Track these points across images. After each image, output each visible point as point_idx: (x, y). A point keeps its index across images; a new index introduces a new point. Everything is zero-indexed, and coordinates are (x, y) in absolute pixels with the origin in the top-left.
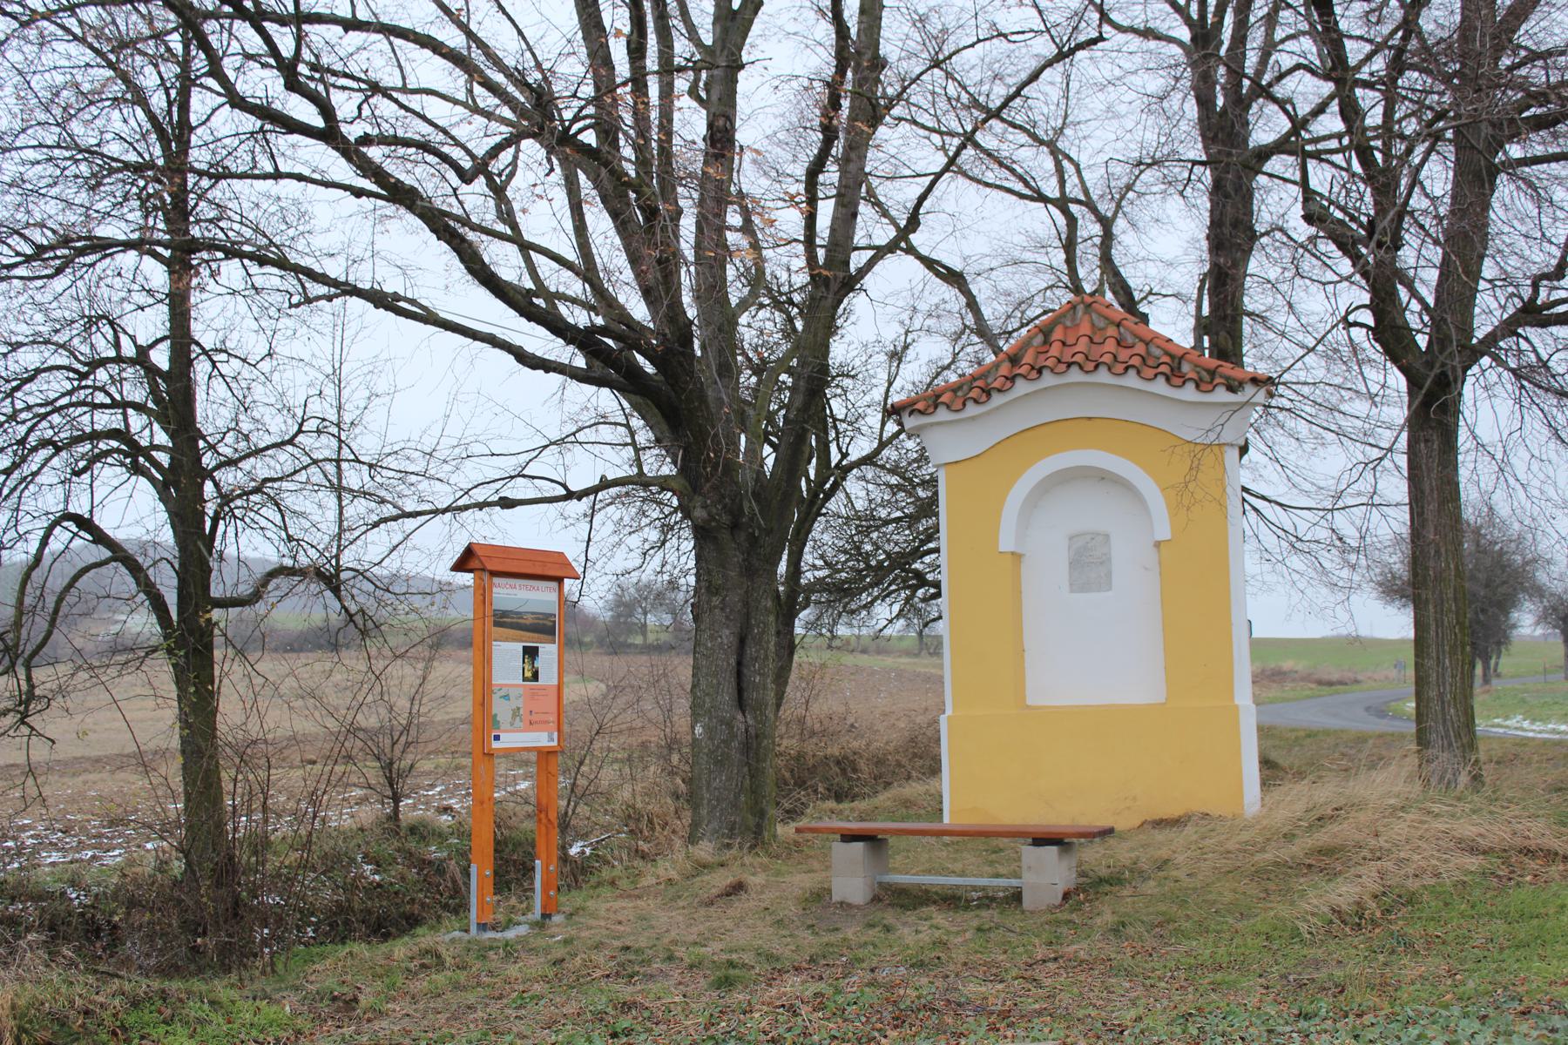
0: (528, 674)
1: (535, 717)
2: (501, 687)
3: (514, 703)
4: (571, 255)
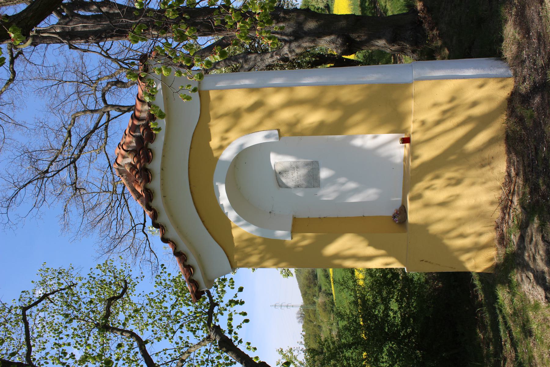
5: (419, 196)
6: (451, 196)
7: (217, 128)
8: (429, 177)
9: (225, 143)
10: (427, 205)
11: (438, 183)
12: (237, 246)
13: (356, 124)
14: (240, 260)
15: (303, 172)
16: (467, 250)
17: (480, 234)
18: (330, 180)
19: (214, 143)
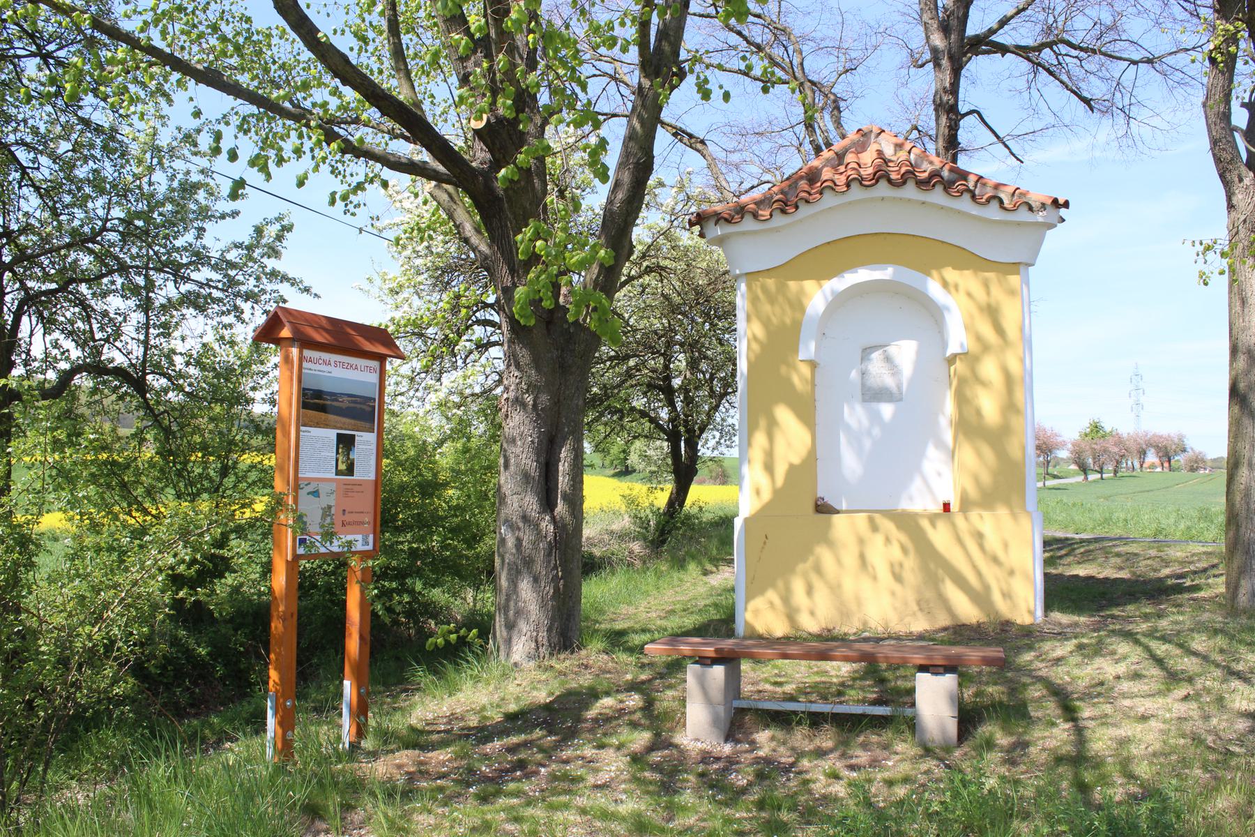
0: (342, 467)
1: (348, 518)
2: (309, 481)
3: (325, 501)
4: (994, 38)
5: (874, 528)
6: (873, 568)
7: (968, 280)
8: (903, 538)
9: (952, 290)
10: (861, 541)
11: (896, 553)
12: (787, 286)
13: (979, 454)
14: (765, 289)
15: (889, 382)
16: (786, 599)
17: (812, 613)
18: (876, 417)
19: (950, 274)
